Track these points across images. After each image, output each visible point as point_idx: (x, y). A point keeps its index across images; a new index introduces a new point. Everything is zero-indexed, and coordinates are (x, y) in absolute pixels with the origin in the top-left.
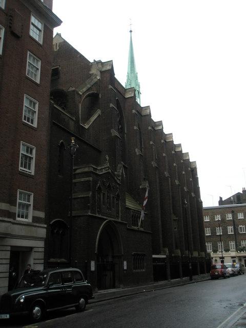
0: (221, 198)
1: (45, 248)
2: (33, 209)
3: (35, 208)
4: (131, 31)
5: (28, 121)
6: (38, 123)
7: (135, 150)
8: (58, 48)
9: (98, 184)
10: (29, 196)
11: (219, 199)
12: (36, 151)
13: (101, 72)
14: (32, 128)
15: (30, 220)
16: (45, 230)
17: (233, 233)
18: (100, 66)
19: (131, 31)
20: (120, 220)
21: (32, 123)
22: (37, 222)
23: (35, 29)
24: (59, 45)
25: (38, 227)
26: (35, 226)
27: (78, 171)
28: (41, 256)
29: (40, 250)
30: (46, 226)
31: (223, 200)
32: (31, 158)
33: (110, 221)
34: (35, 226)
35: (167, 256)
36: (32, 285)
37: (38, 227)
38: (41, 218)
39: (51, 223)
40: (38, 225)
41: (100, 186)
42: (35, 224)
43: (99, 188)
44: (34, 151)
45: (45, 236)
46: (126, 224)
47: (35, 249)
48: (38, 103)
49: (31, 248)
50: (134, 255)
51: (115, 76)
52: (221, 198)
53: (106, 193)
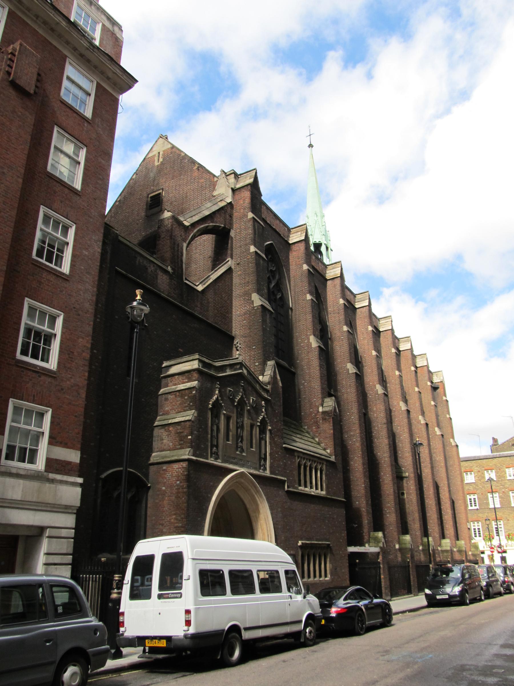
0: (495, 440)
1: (77, 528)
2: (50, 443)
3: (53, 441)
4: (311, 146)
5: (49, 259)
6: (72, 266)
7: (309, 339)
8: (161, 160)
9: (215, 398)
10: (41, 415)
11: (491, 442)
12: (65, 321)
13: (234, 190)
14: (60, 276)
15: (40, 465)
16: (79, 490)
17: (468, 497)
18: (232, 178)
19: (311, 146)
20: (268, 473)
21: (61, 267)
22: (58, 471)
23: (74, 89)
24: (163, 155)
25: (62, 482)
26: (53, 481)
27: (173, 370)
28: (67, 546)
29: (64, 533)
30: (80, 480)
31: (500, 442)
32: (49, 338)
33: (242, 472)
34: (53, 481)
35: (381, 548)
36: (44, 608)
37: (62, 482)
38: (69, 463)
39: (103, 476)
40: (59, 477)
41: (217, 398)
42: (51, 476)
43: (216, 404)
44: (59, 322)
45: (78, 504)
46: (283, 482)
47: (47, 533)
48: (74, 228)
49: (41, 530)
50: (303, 547)
51: (262, 198)
52: (495, 440)
53: (234, 415)
